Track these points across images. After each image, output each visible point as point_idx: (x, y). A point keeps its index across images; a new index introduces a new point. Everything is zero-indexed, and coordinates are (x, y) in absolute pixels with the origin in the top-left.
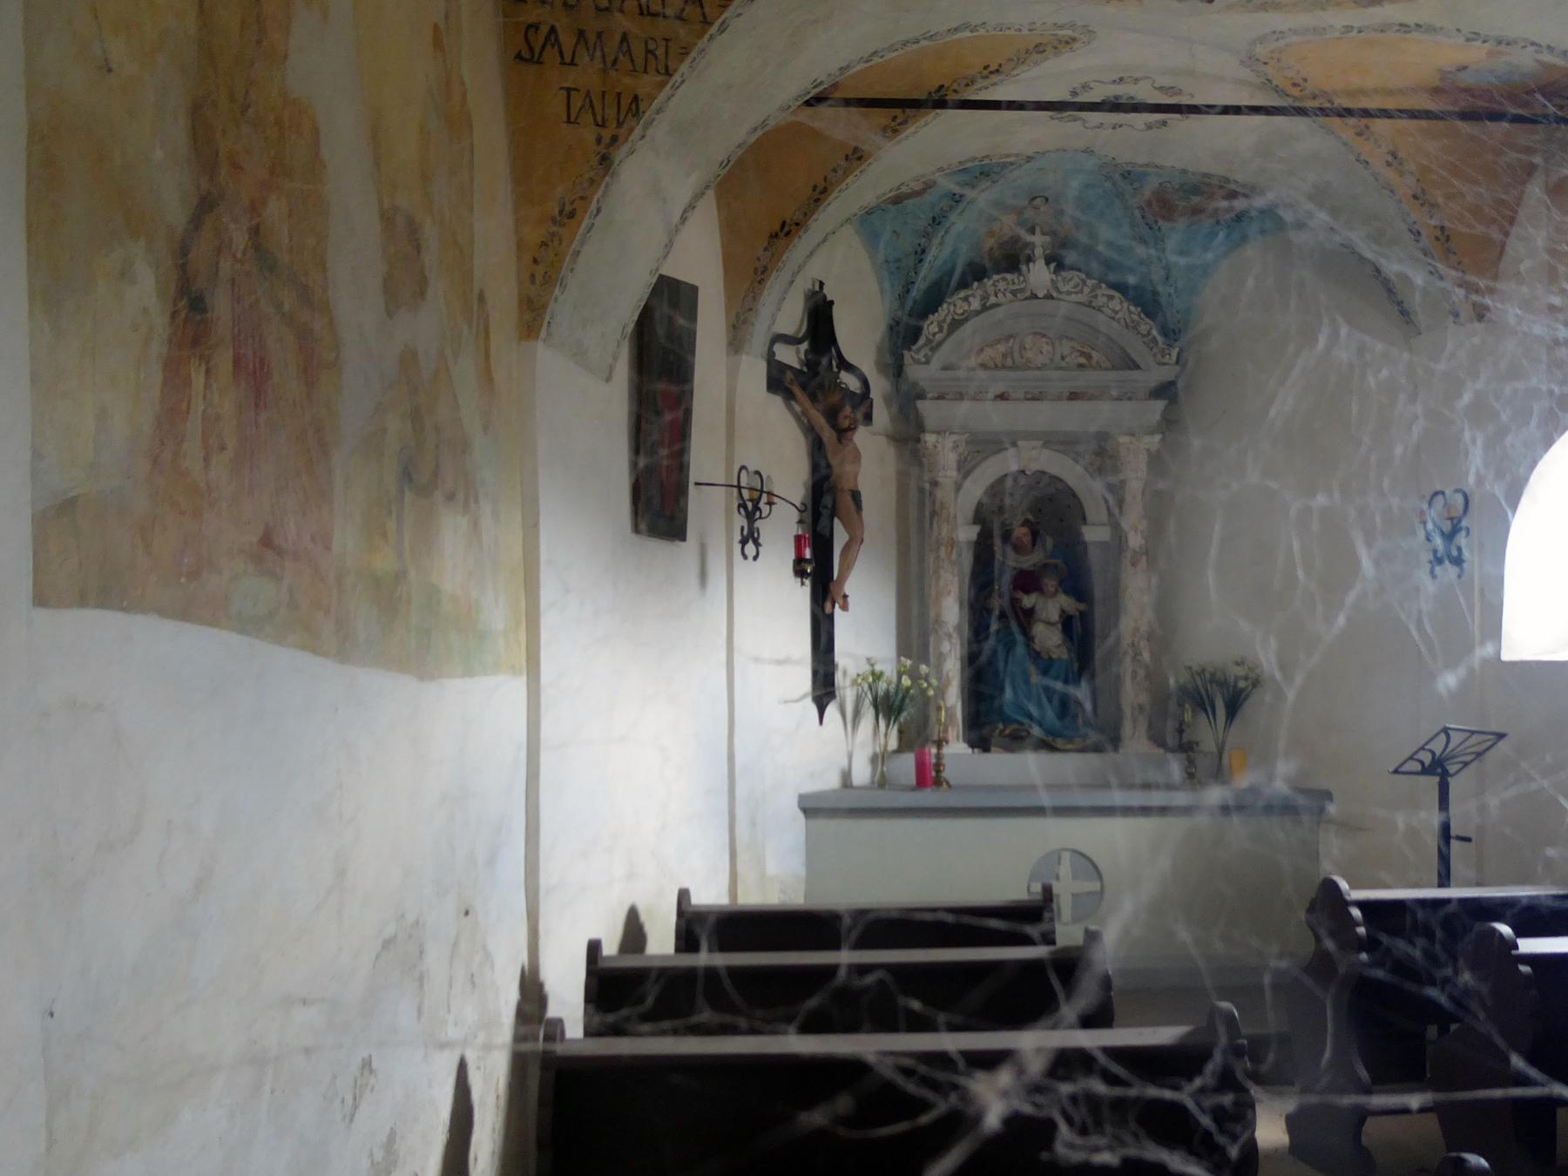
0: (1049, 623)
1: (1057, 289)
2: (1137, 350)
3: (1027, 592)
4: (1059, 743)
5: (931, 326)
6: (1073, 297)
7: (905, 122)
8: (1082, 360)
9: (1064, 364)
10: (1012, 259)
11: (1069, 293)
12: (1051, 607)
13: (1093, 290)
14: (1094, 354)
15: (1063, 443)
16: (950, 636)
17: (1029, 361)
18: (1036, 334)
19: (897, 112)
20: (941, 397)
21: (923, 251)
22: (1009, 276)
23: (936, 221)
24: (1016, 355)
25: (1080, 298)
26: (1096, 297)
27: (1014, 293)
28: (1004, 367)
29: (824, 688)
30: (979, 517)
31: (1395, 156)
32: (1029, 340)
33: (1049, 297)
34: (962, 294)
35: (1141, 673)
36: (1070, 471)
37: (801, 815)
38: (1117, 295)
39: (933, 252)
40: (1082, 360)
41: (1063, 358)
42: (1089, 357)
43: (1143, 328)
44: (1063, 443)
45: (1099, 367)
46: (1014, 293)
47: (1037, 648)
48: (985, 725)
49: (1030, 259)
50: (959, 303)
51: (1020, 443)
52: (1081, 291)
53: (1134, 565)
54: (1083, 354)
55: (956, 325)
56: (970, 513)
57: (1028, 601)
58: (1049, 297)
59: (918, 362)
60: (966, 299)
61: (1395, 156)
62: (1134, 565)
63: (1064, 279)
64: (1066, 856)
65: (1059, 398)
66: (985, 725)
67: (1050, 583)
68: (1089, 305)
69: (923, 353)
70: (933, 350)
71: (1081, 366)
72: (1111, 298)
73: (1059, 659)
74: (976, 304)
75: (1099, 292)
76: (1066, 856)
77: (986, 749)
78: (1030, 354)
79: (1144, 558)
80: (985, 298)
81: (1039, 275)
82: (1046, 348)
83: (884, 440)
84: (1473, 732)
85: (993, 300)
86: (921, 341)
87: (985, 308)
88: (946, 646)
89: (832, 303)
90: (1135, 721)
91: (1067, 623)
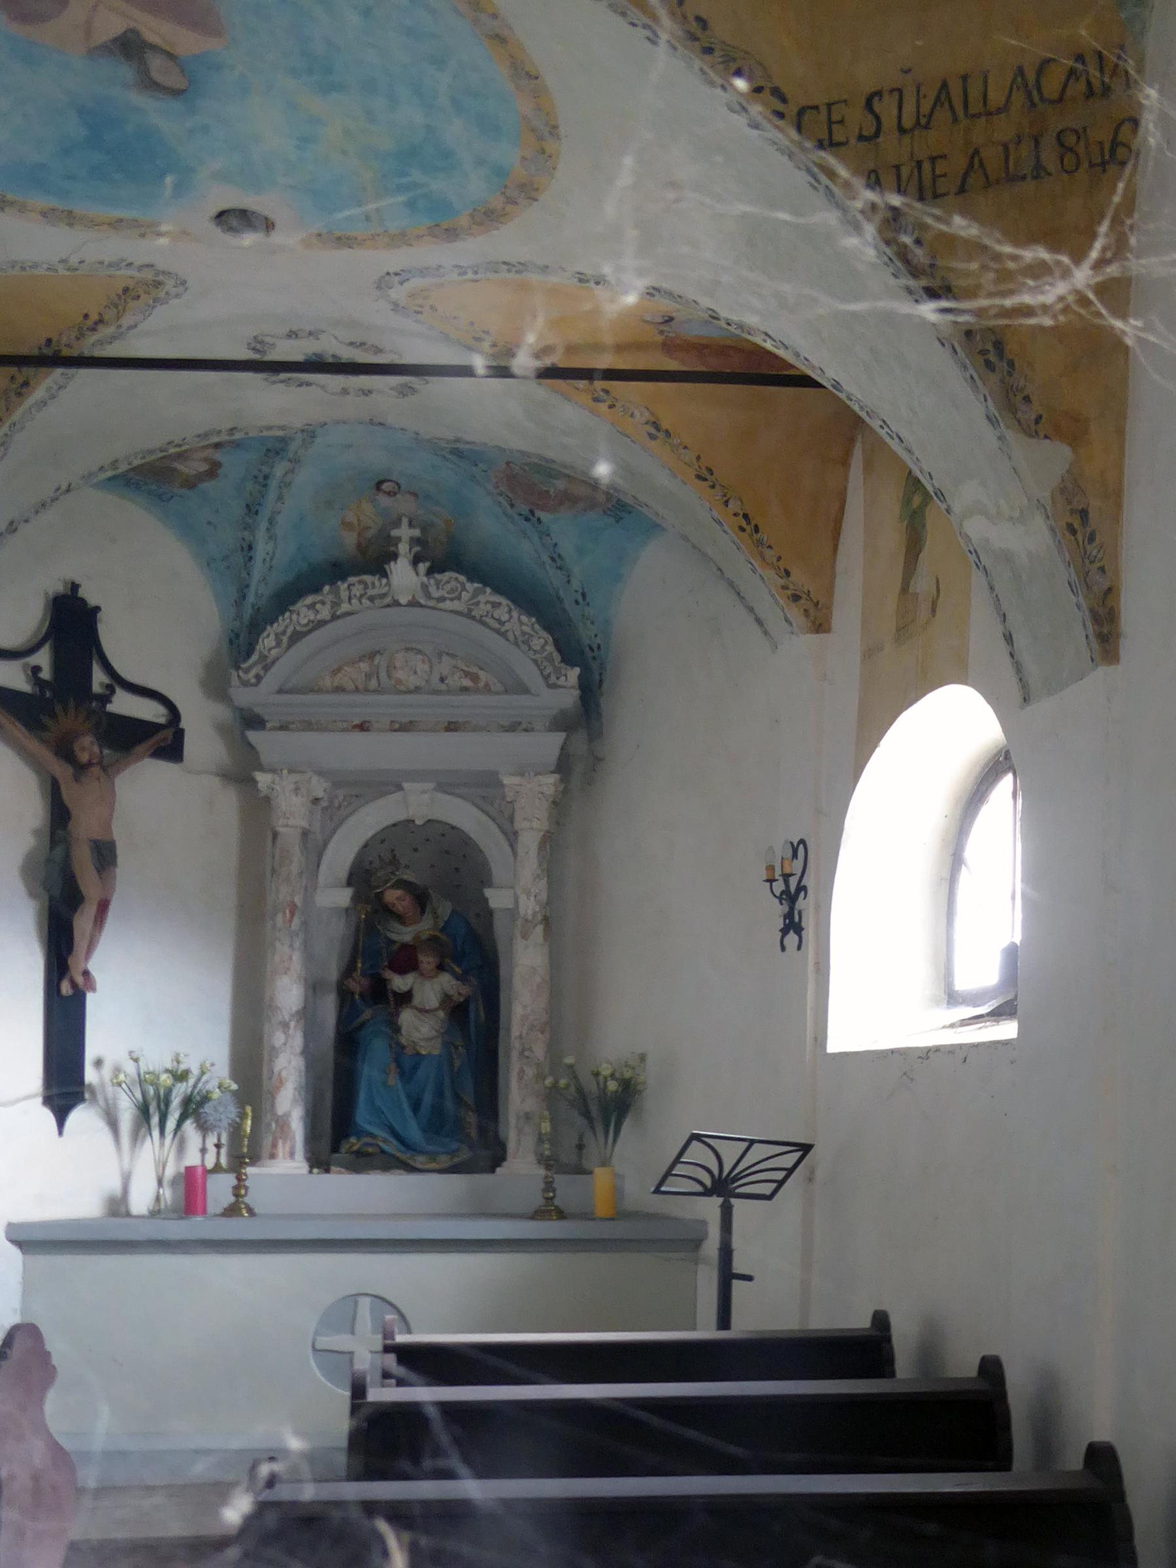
0: (423, 1011)
1: (428, 596)
2: (528, 672)
3: (402, 971)
4: (420, 1161)
5: (267, 641)
6: (448, 605)
7: (26, 384)
8: (467, 682)
9: (443, 687)
10: (375, 559)
11: (442, 599)
12: (431, 989)
13: (474, 597)
14: (482, 674)
15: (448, 783)
16: (285, 1026)
17: (399, 682)
18: (407, 649)
19: (13, 370)
20: (283, 727)
21: (250, 547)
22: (367, 578)
23: (252, 509)
24: (383, 674)
25: (456, 605)
26: (478, 603)
27: (371, 599)
28: (367, 691)
29: (64, 1085)
30: (361, 877)
31: (656, 425)
32: (400, 658)
33: (414, 604)
34: (309, 600)
35: (530, 1072)
36: (463, 815)
37: (15, 1252)
38: (504, 601)
39: (262, 548)
40: (467, 682)
41: (442, 680)
42: (475, 678)
43: (536, 643)
44: (448, 783)
45: (487, 689)
46: (371, 599)
47: (403, 1041)
48: (338, 1138)
49: (394, 556)
50: (304, 610)
51: (406, 785)
52: (459, 598)
53: (525, 937)
54: (467, 674)
55: (297, 637)
56: (343, 873)
57: (399, 983)
58: (414, 604)
59: (245, 684)
60: (312, 606)
61: (656, 425)
62: (525, 937)
63: (438, 583)
64: (365, 1304)
65: (433, 730)
66: (338, 1138)
67: (427, 961)
68: (469, 615)
69: (254, 672)
70: (266, 668)
71: (465, 690)
72: (496, 605)
73: (430, 1055)
74: (325, 613)
75: (482, 598)
76: (365, 1304)
77: (327, 1171)
78: (400, 674)
79: (539, 929)
80: (336, 605)
81: (404, 575)
82: (422, 667)
83: (216, 782)
84: (752, 1142)
85: (345, 607)
86: (255, 657)
87: (335, 618)
88: (279, 1038)
89: (97, 609)
90: (520, 1131)
91: (457, 1012)
